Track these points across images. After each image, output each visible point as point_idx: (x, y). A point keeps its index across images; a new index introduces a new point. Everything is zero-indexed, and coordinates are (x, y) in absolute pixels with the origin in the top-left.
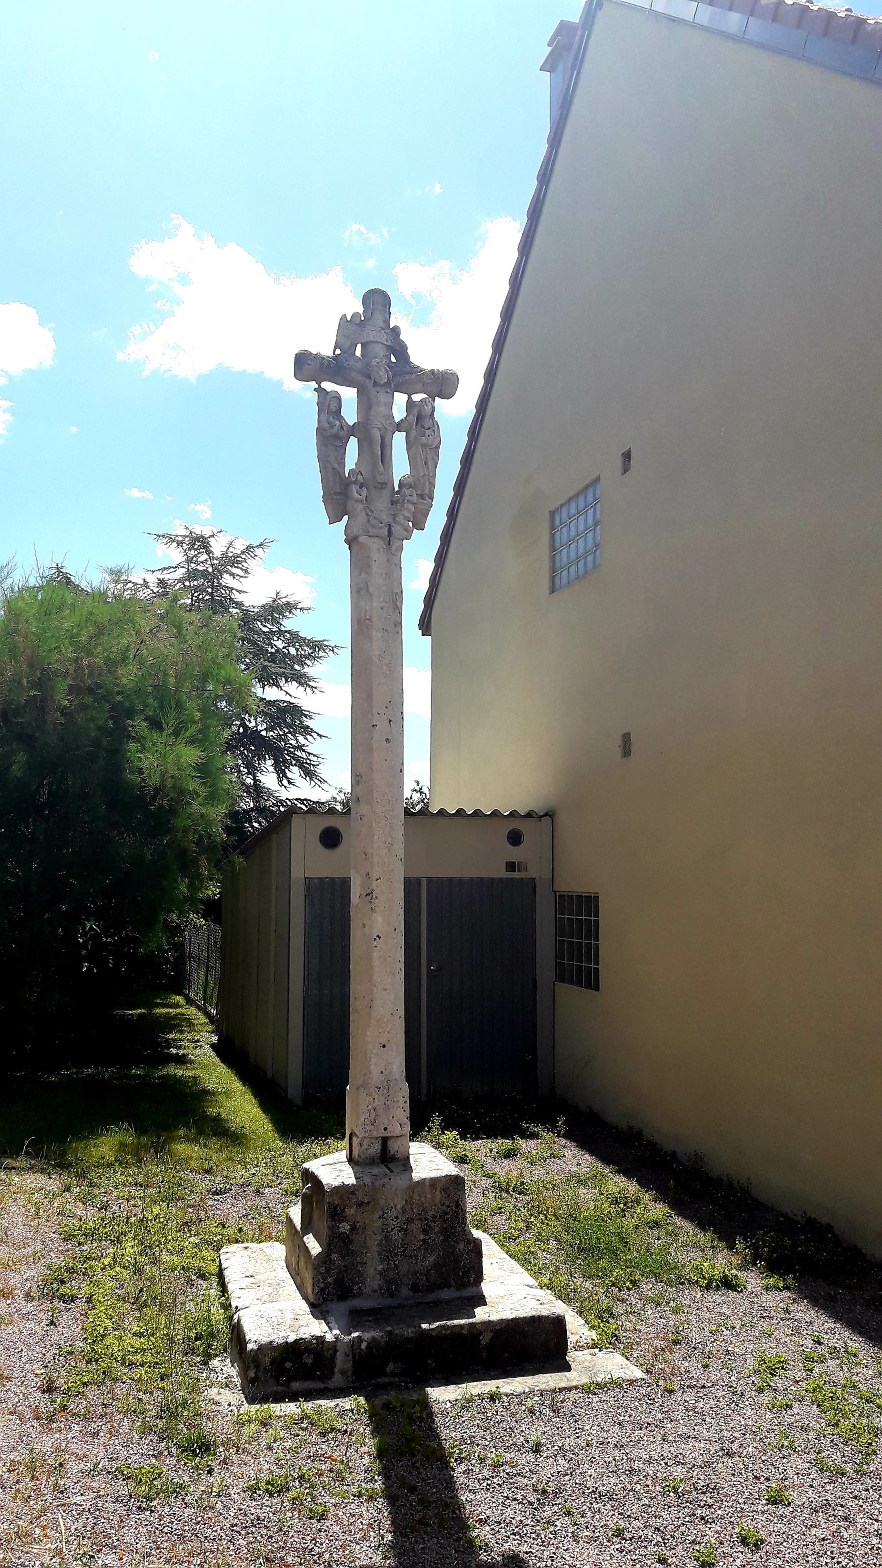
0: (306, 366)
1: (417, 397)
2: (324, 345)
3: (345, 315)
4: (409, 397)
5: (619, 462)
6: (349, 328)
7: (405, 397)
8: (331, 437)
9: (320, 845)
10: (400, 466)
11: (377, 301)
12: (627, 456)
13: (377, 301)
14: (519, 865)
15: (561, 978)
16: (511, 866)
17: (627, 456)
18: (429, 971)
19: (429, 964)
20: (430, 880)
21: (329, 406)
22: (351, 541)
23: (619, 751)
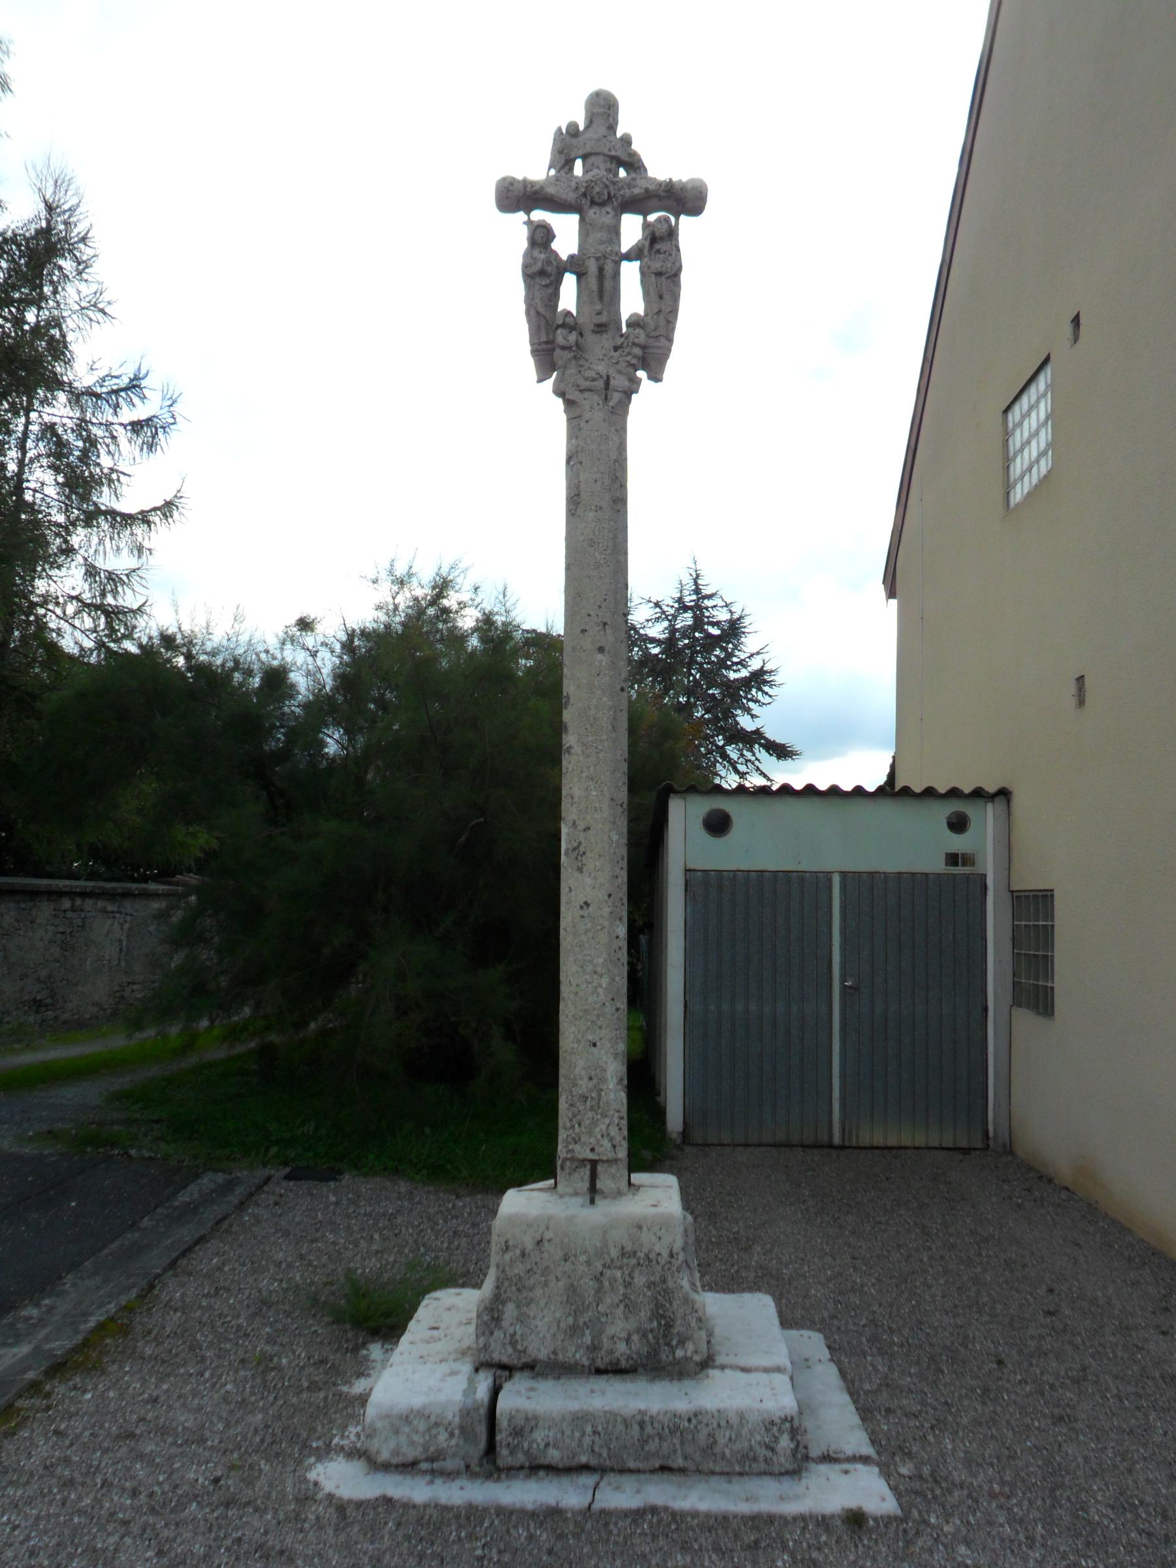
0: (516, 196)
1: (652, 218)
2: (536, 167)
3: (560, 129)
4: (645, 218)
5: (1068, 329)
6: (567, 146)
7: (639, 219)
8: (542, 272)
9: (723, 839)
10: (632, 299)
11: (603, 108)
12: (1076, 321)
13: (603, 108)
14: (963, 859)
15: (1017, 1002)
16: (952, 859)
17: (1076, 321)
18: (844, 989)
19: (843, 979)
20: (844, 875)
21: (541, 237)
22: (559, 392)
23: (1073, 702)
